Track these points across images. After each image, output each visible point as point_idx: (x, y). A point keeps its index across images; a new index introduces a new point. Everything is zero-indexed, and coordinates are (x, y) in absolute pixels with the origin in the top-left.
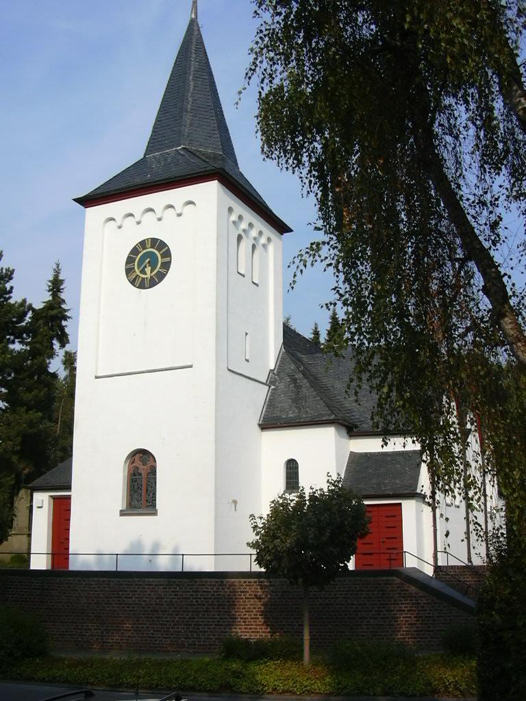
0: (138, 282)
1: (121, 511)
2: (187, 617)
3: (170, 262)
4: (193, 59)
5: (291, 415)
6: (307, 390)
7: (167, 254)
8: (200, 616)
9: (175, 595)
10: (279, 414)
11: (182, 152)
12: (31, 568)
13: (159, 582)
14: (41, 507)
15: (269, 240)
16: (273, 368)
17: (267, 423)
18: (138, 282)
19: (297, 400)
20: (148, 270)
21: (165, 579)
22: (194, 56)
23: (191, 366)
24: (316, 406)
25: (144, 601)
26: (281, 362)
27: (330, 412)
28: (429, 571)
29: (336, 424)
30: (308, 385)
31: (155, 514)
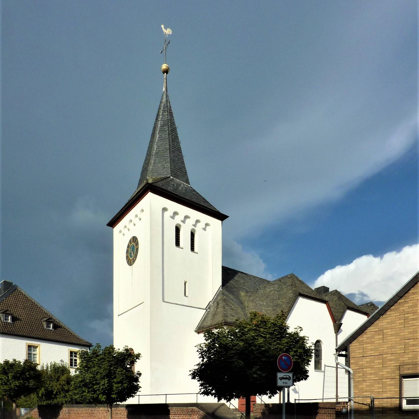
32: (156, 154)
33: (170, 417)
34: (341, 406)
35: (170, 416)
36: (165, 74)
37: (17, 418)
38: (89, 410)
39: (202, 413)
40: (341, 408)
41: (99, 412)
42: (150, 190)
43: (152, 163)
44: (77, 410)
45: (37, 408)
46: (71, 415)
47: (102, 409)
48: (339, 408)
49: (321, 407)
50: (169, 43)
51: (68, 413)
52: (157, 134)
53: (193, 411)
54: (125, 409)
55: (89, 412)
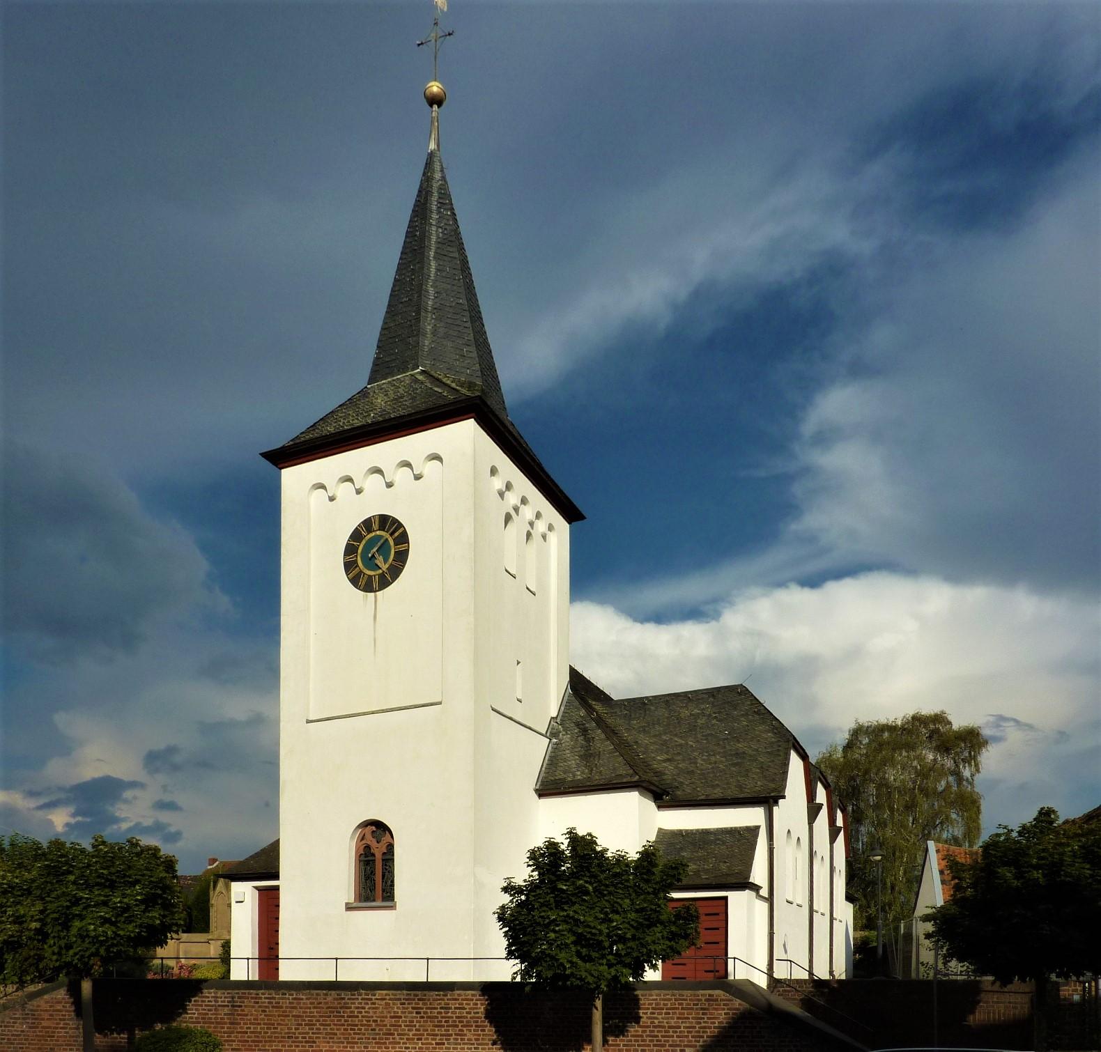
0: (362, 582)
1: (347, 904)
2: (434, 1042)
3: (407, 551)
4: (434, 223)
5: (579, 777)
6: (601, 743)
7: (403, 538)
8: (452, 1041)
9: (417, 1013)
10: (563, 776)
11: (420, 377)
12: (231, 979)
13: (395, 995)
14: (242, 902)
15: (551, 528)
16: (555, 715)
17: (548, 787)
18: (362, 582)
19: (588, 756)
20: (379, 561)
21: (405, 992)
22: (435, 216)
23: (440, 703)
24: (612, 764)
25: (374, 1021)
26: (567, 706)
27: (631, 771)
28: (762, 981)
29: (640, 789)
30: (603, 736)
31: (393, 907)
32: (435, 311)
33: (641, 1015)
34: (1070, 989)
35: (641, 1011)
36: (435, 107)
37: (217, 1045)
38: (329, 999)
39: (739, 1004)
40: (1071, 992)
41: (374, 1004)
42: (476, 415)
43: (428, 330)
44: (274, 998)
45: (65, 988)
46: (243, 1011)
47: (386, 995)
48: (1067, 993)
49: (986, 989)
50: (450, 34)
51: (228, 1006)
52: (431, 258)
53: (713, 1000)
54: (479, 996)
55: (327, 1003)
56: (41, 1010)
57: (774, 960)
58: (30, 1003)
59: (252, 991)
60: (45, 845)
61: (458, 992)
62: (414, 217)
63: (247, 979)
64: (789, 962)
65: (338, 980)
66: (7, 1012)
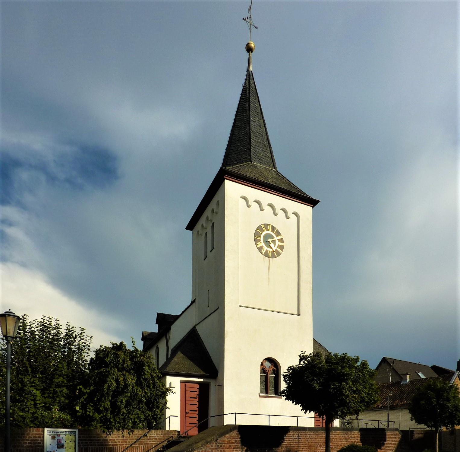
45: (237, 431)
56: (225, 443)
57: (179, 415)
58: (220, 439)
59: (304, 432)
60: (373, 365)
61: (354, 432)
62: (244, 90)
63: (235, 424)
64: (392, 422)
65: (270, 425)
66: (208, 445)
